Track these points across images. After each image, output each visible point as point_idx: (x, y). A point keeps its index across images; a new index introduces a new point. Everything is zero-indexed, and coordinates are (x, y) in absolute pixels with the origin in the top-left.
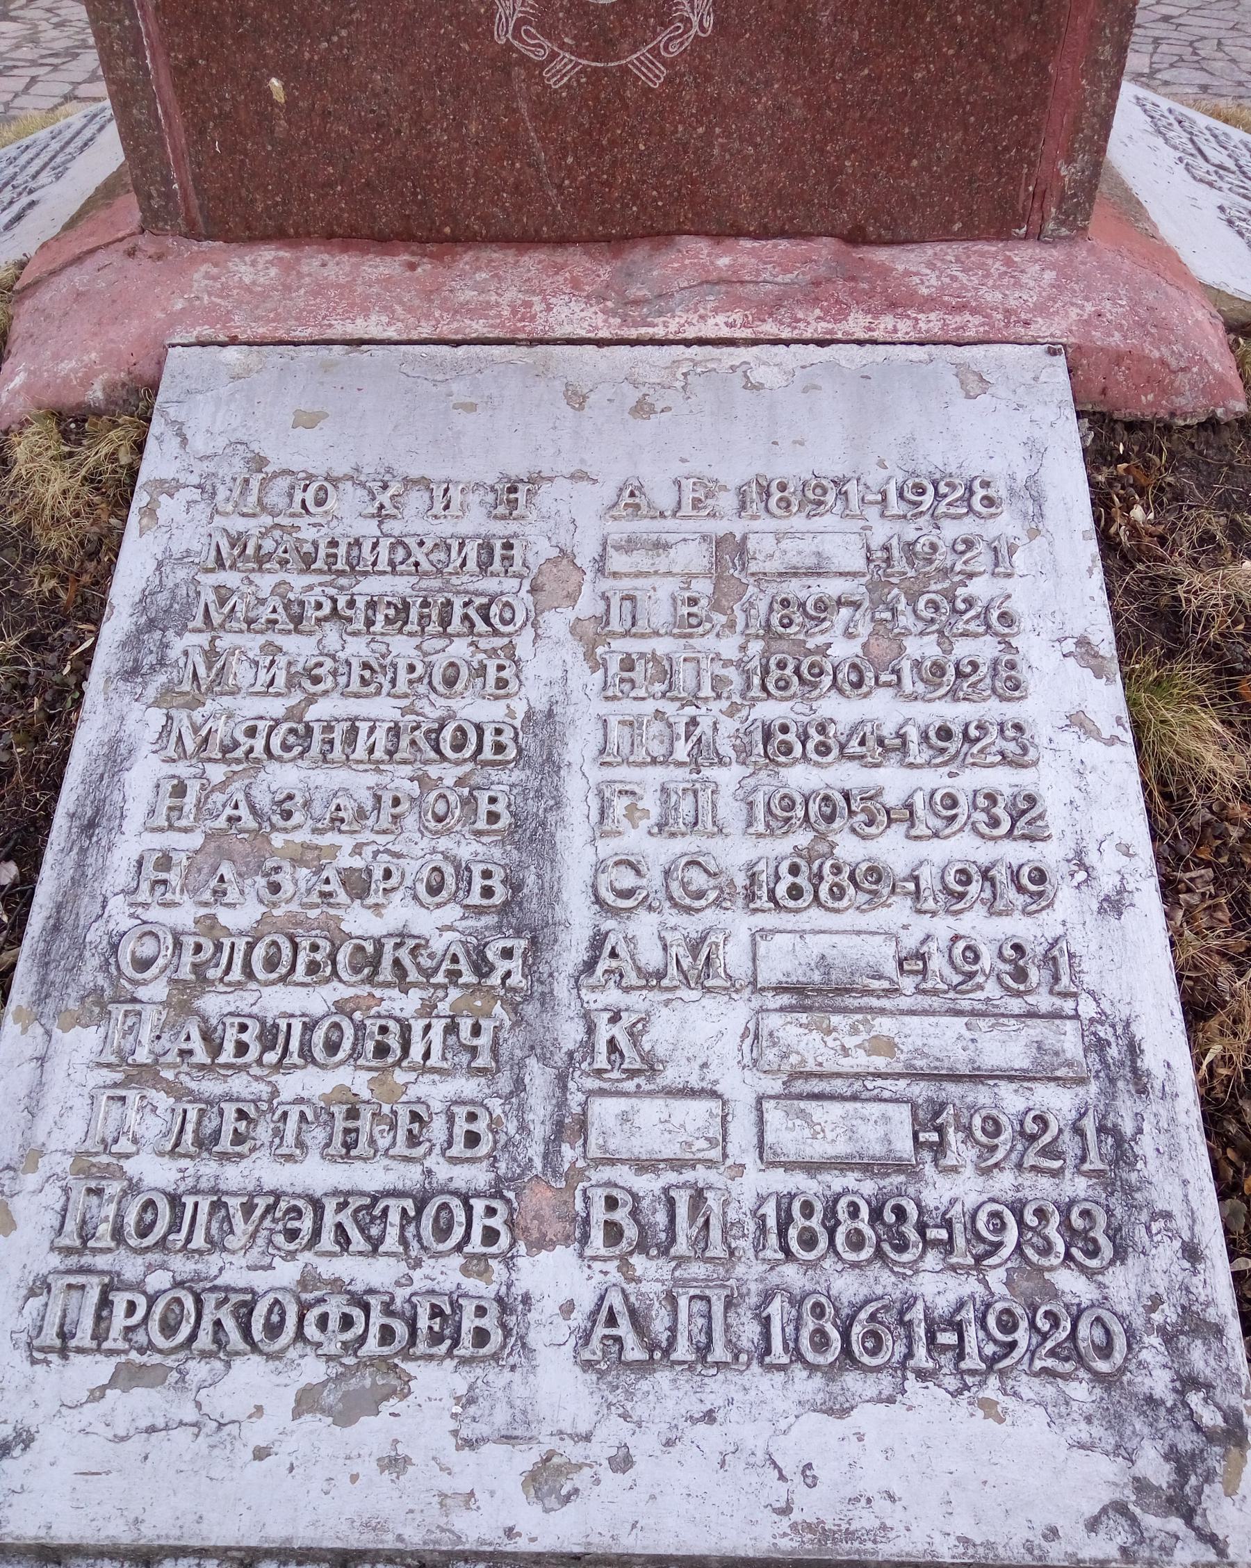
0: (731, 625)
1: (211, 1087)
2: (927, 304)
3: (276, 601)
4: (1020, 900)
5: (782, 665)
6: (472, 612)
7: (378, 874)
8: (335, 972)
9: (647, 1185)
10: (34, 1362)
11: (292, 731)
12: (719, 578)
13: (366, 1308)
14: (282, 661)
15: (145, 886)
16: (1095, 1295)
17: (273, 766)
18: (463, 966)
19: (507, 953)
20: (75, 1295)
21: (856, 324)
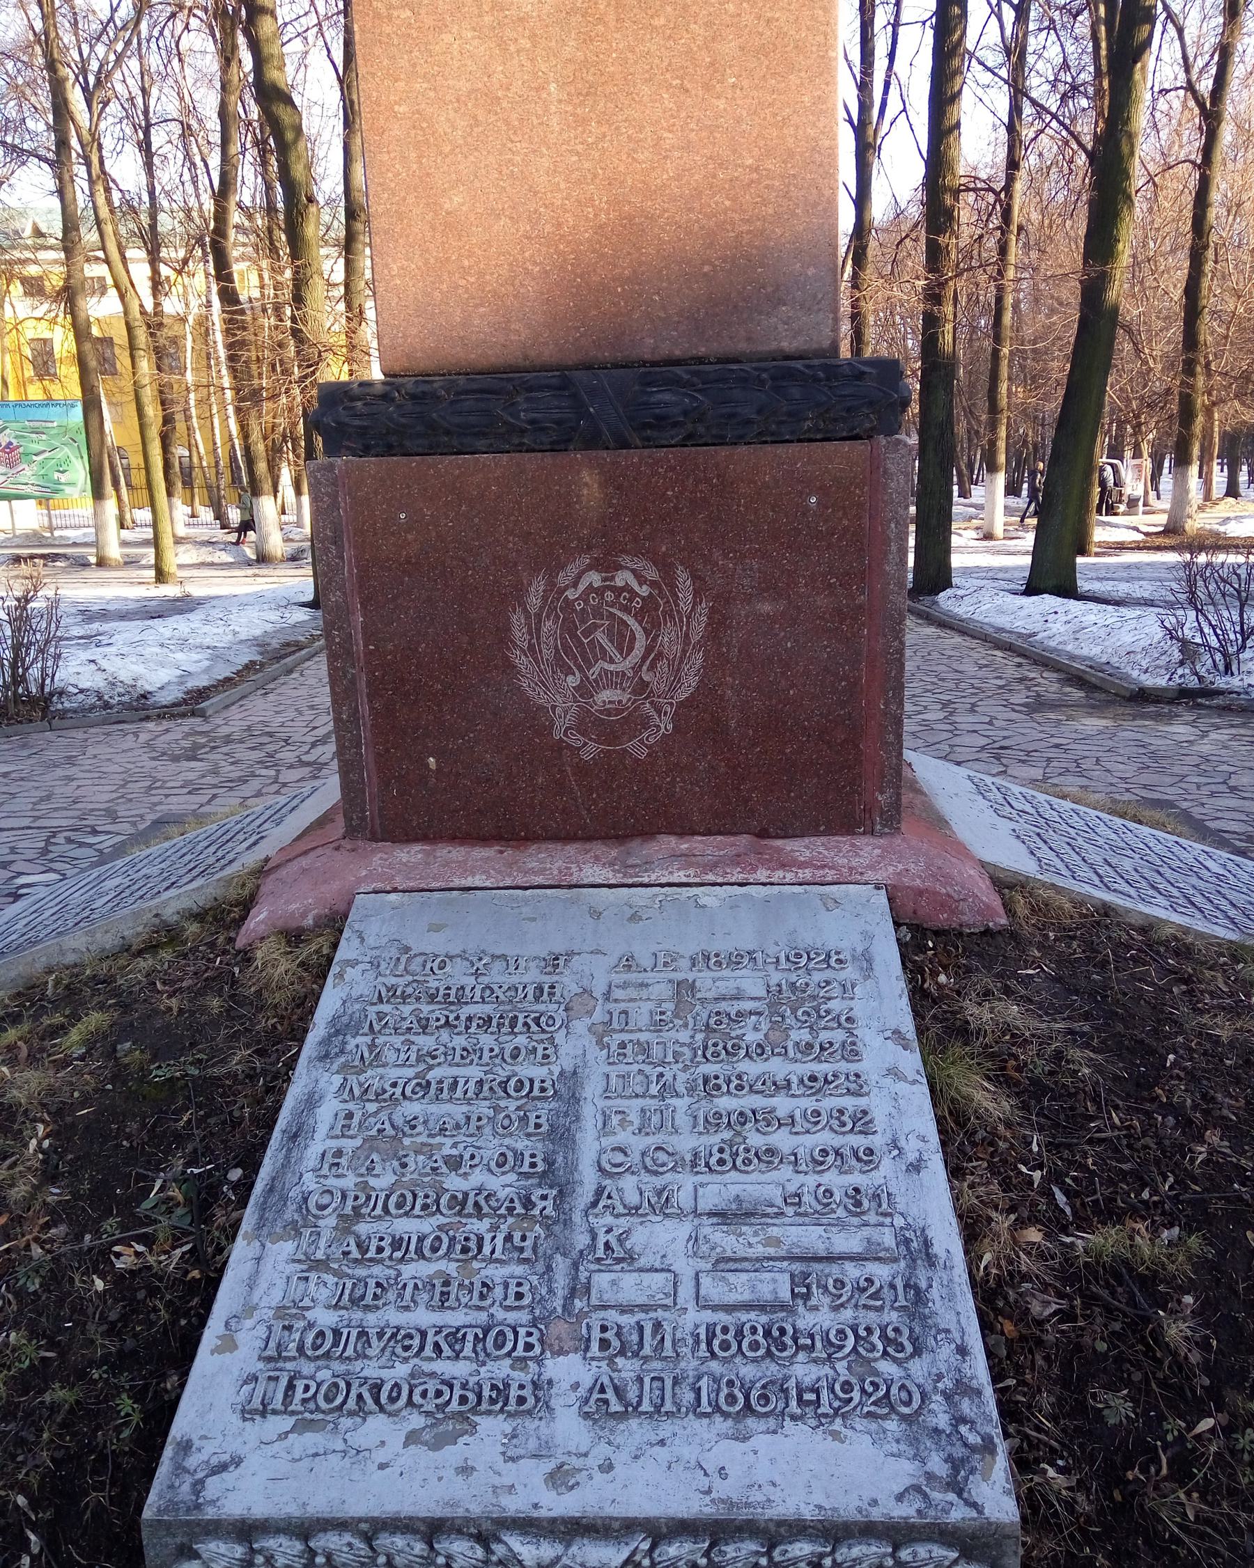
0: (686, 1025)
1: (361, 1272)
2: (802, 865)
3: (413, 1018)
4: (858, 1166)
5: (715, 1045)
6: (529, 1021)
7: (467, 1156)
8: (438, 1209)
9: (627, 1320)
10: (245, 1420)
11: (418, 1084)
12: (679, 1002)
13: (451, 1387)
14: (414, 1048)
15: (326, 1166)
16: (903, 1374)
17: (406, 1103)
18: (517, 1204)
19: (544, 1197)
20: (272, 1384)
21: (762, 875)
